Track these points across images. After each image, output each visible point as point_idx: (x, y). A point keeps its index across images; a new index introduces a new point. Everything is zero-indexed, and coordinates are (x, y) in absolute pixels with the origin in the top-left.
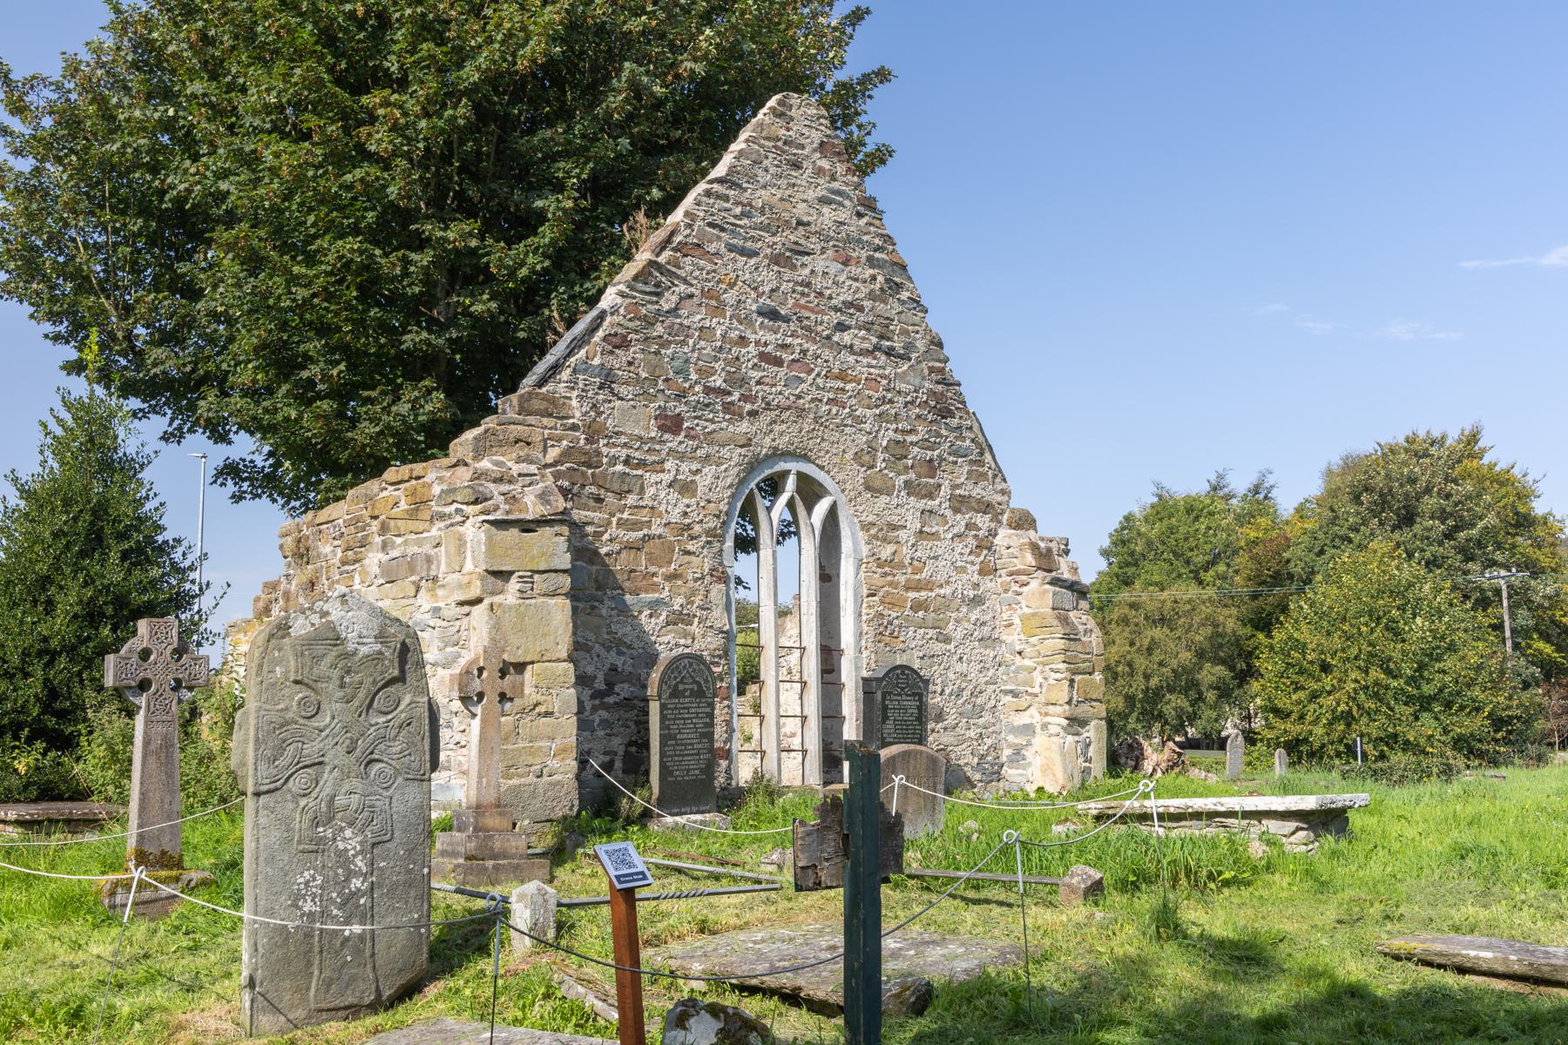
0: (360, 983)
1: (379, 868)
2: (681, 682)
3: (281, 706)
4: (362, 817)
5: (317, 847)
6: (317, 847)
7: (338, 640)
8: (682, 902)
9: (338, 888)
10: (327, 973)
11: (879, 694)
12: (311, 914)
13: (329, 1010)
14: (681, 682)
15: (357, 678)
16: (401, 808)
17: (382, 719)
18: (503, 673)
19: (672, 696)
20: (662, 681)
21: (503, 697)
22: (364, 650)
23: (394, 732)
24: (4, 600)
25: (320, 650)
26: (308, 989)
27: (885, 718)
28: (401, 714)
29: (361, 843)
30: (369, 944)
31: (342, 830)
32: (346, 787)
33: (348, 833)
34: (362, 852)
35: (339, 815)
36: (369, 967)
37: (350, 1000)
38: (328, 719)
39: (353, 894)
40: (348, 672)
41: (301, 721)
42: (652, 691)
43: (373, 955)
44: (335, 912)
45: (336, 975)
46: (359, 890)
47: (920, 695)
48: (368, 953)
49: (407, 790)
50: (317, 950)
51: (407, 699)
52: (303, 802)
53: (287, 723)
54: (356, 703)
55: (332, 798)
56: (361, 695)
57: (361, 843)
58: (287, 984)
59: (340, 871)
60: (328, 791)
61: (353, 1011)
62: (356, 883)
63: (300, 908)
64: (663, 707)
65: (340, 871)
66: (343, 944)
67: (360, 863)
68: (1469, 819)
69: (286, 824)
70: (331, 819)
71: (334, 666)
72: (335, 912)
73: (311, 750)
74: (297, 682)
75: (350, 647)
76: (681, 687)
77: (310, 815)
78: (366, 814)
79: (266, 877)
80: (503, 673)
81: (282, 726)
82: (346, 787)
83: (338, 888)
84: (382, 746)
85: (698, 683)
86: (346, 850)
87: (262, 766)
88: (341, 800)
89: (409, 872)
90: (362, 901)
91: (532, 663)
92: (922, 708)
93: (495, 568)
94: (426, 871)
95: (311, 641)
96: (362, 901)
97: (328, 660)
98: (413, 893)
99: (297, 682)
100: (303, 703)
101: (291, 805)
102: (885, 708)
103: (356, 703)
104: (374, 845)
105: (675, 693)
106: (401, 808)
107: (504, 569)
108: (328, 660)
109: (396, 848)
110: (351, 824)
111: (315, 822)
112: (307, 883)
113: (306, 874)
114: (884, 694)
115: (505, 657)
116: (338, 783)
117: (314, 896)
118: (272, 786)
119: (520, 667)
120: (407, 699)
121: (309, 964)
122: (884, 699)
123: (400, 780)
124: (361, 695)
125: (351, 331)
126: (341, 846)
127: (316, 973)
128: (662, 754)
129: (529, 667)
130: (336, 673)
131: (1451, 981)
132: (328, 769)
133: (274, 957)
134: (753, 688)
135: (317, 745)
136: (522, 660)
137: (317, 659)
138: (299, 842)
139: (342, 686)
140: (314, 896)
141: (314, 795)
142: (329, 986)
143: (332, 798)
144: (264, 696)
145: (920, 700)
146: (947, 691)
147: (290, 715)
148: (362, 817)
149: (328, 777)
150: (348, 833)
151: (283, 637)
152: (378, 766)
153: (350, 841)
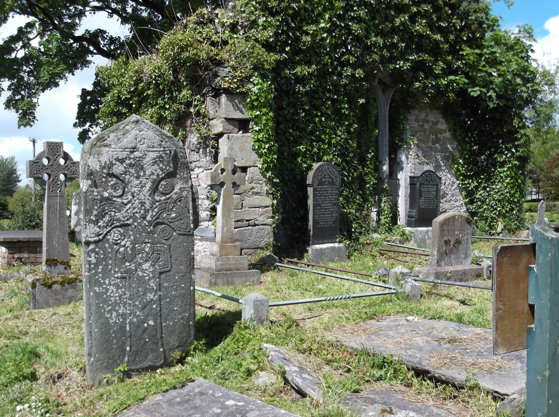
2: (324, 177)
9: (139, 299)
11: (418, 184)
14: (324, 177)
17: (163, 198)
18: (234, 172)
19: (319, 184)
20: (314, 177)
21: (235, 185)
27: (421, 196)
30: (159, 331)
31: (140, 264)
42: (309, 181)
46: (152, 300)
47: (437, 185)
59: (140, 289)
64: (315, 190)
66: (143, 332)
76: (323, 180)
78: (154, 255)
80: (234, 172)
85: (332, 178)
91: (250, 167)
92: (438, 191)
93: (230, 117)
96: (154, 306)
102: (420, 192)
104: (161, 273)
105: (321, 183)
107: (535, 315)
114: (420, 184)
115: (236, 164)
119: (244, 169)
122: (420, 187)
128: (314, 213)
129: (249, 169)
134: (115, 119)
136: (244, 165)
145: (437, 187)
146: (447, 183)
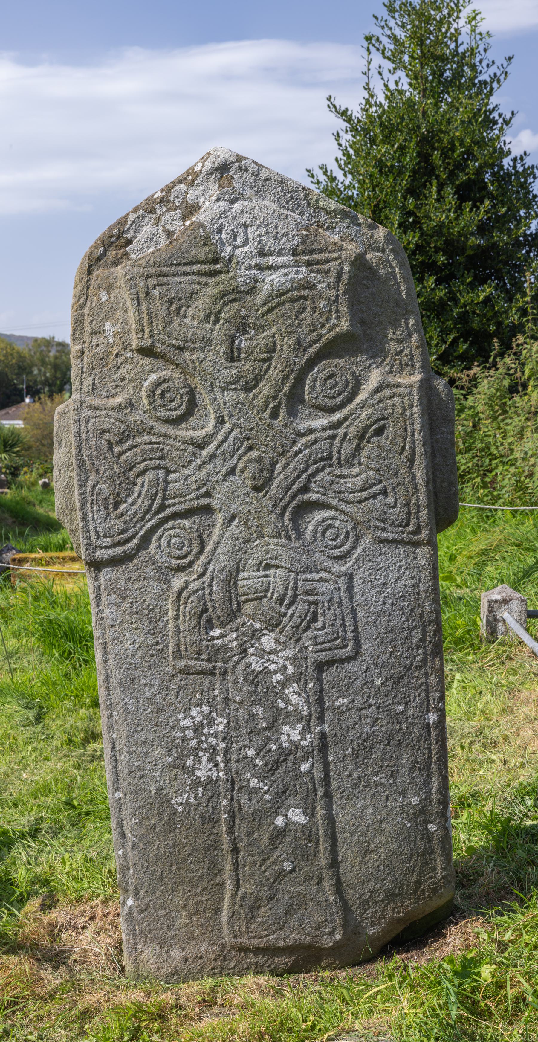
0: (313, 910)
1: (334, 710)
3: (119, 400)
4: (296, 612)
5: (212, 666)
6: (212, 666)
9: (257, 741)
10: (247, 888)
12: (210, 783)
13: (258, 951)
15: (261, 339)
16: (373, 597)
17: (324, 421)
22: (272, 281)
23: (347, 448)
25: (181, 284)
26: (217, 911)
29: (294, 660)
30: (323, 845)
31: (255, 634)
32: (257, 554)
33: (268, 641)
34: (298, 677)
35: (248, 608)
36: (327, 884)
37: (292, 937)
38: (212, 423)
40: (243, 328)
41: (160, 428)
43: (334, 864)
44: (253, 782)
48: (323, 859)
49: (383, 561)
50: (226, 845)
51: (373, 379)
52: (178, 582)
54: (265, 389)
56: (274, 374)
57: (294, 660)
58: (179, 898)
59: (258, 710)
60: (221, 562)
61: (304, 959)
62: (291, 733)
63: (191, 772)
65: (258, 710)
67: (295, 697)
68: (484, 694)
69: (151, 619)
70: (234, 614)
71: (212, 317)
72: (253, 782)
74: (146, 352)
75: (242, 275)
77: (194, 604)
78: (301, 607)
79: (126, 712)
81: (124, 437)
82: (257, 554)
83: (257, 741)
84: (324, 477)
86: (266, 672)
87: (96, 514)
88: (248, 580)
89: (398, 718)
90: (305, 767)
94: (432, 717)
95: (162, 269)
96: (305, 767)
97: (200, 305)
98: (406, 758)
100: (159, 392)
101: (155, 586)
103: (265, 389)
104: (321, 666)
106: (373, 597)
108: (200, 305)
110: (273, 625)
112: (198, 728)
113: (195, 712)
116: (243, 545)
117: (213, 751)
118: (118, 551)
120: (373, 379)
121: (215, 869)
123: (366, 542)
124: (274, 374)
125: (432, 41)
126: (256, 664)
127: (229, 886)
130: (219, 332)
132: (219, 519)
133: (151, 853)
137: (178, 304)
138: (178, 654)
139: (233, 356)
140: (213, 751)
141: (197, 568)
147: (135, 418)
148: (296, 612)
150: (268, 641)
151: (116, 263)
152: (319, 515)
153: (273, 656)
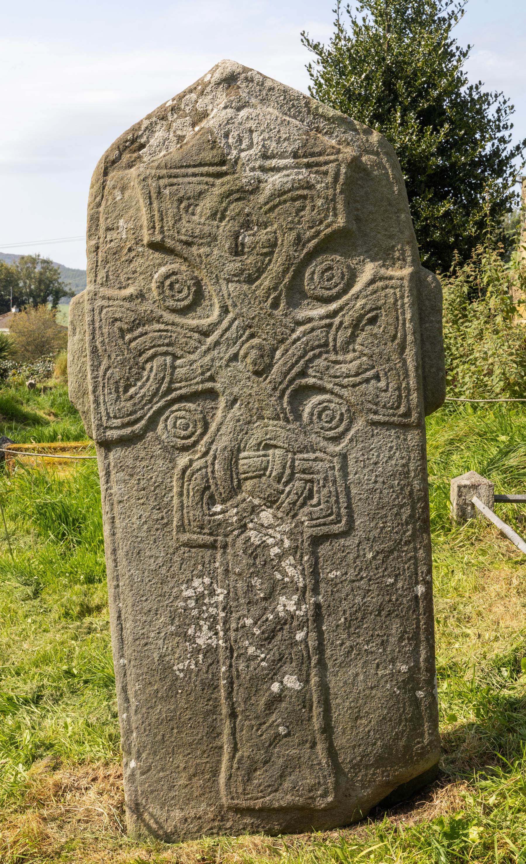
1: (328, 582)
3: (130, 290)
6: (212, 540)
7: (222, 165)
8: (351, 469)
9: (255, 611)
15: (263, 235)
16: (365, 475)
17: (321, 310)
22: (274, 181)
23: (342, 336)
24: (85, 861)
25: (190, 185)
26: (215, 773)
28: (357, 299)
29: (291, 534)
30: (316, 710)
31: (254, 510)
32: (257, 434)
33: (266, 516)
35: (248, 485)
38: (216, 312)
39: (281, 623)
40: (247, 225)
41: (168, 317)
45: (261, 756)
48: (317, 723)
49: (375, 442)
50: (225, 710)
52: (182, 460)
53: (138, 322)
54: (266, 281)
55: (234, 455)
56: (276, 266)
57: (291, 534)
58: (180, 760)
59: (256, 582)
61: (295, 821)
62: (286, 604)
65: (256, 582)
67: (291, 569)
69: (157, 494)
71: (218, 215)
73: (190, 366)
75: (246, 176)
78: (298, 484)
82: (257, 434)
84: (321, 363)
86: (264, 546)
88: (249, 460)
90: (299, 636)
94: (420, 589)
96: (299, 636)
97: (207, 204)
98: (395, 628)
99: (154, 246)
103: (266, 281)
104: (316, 541)
106: (365, 475)
108: (207, 204)
109: (359, 547)
110: (271, 502)
111: (207, 495)
112: (199, 598)
113: (196, 583)
121: (214, 733)
123: (359, 424)
124: (276, 266)
127: (227, 749)
130: (225, 228)
131: (415, 395)
132: (222, 402)
135: (198, 360)
137: (188, 202)
138: (182, 528)
139: (237, 250)
141: (201, 448)
142: (251, 772)
143: (234, 455)
144: (102, 274)
147: (146, 307)
149: (224, 418)
150: (266, 516)
153: (271, 530)
